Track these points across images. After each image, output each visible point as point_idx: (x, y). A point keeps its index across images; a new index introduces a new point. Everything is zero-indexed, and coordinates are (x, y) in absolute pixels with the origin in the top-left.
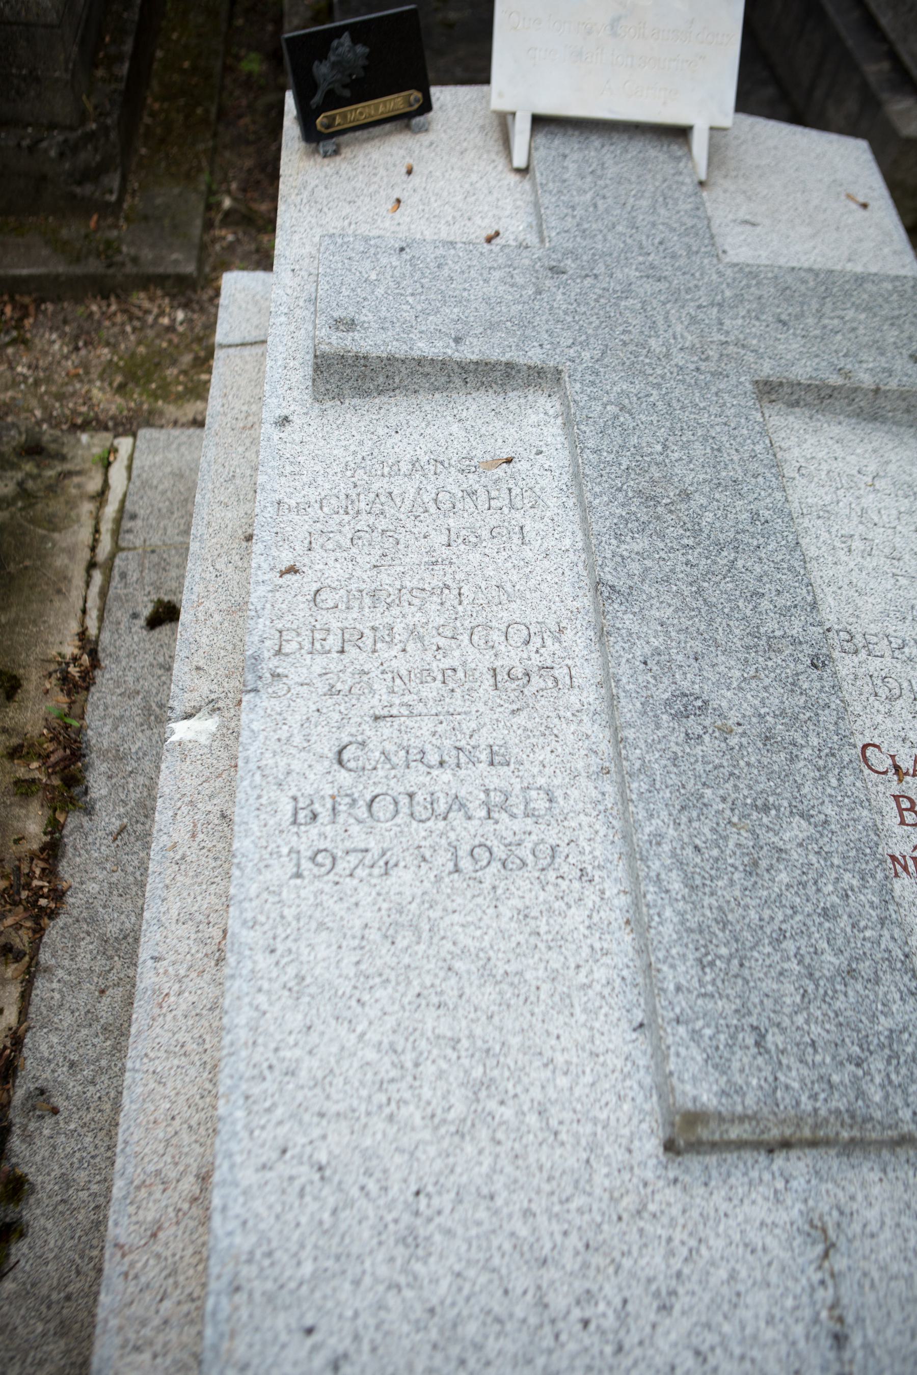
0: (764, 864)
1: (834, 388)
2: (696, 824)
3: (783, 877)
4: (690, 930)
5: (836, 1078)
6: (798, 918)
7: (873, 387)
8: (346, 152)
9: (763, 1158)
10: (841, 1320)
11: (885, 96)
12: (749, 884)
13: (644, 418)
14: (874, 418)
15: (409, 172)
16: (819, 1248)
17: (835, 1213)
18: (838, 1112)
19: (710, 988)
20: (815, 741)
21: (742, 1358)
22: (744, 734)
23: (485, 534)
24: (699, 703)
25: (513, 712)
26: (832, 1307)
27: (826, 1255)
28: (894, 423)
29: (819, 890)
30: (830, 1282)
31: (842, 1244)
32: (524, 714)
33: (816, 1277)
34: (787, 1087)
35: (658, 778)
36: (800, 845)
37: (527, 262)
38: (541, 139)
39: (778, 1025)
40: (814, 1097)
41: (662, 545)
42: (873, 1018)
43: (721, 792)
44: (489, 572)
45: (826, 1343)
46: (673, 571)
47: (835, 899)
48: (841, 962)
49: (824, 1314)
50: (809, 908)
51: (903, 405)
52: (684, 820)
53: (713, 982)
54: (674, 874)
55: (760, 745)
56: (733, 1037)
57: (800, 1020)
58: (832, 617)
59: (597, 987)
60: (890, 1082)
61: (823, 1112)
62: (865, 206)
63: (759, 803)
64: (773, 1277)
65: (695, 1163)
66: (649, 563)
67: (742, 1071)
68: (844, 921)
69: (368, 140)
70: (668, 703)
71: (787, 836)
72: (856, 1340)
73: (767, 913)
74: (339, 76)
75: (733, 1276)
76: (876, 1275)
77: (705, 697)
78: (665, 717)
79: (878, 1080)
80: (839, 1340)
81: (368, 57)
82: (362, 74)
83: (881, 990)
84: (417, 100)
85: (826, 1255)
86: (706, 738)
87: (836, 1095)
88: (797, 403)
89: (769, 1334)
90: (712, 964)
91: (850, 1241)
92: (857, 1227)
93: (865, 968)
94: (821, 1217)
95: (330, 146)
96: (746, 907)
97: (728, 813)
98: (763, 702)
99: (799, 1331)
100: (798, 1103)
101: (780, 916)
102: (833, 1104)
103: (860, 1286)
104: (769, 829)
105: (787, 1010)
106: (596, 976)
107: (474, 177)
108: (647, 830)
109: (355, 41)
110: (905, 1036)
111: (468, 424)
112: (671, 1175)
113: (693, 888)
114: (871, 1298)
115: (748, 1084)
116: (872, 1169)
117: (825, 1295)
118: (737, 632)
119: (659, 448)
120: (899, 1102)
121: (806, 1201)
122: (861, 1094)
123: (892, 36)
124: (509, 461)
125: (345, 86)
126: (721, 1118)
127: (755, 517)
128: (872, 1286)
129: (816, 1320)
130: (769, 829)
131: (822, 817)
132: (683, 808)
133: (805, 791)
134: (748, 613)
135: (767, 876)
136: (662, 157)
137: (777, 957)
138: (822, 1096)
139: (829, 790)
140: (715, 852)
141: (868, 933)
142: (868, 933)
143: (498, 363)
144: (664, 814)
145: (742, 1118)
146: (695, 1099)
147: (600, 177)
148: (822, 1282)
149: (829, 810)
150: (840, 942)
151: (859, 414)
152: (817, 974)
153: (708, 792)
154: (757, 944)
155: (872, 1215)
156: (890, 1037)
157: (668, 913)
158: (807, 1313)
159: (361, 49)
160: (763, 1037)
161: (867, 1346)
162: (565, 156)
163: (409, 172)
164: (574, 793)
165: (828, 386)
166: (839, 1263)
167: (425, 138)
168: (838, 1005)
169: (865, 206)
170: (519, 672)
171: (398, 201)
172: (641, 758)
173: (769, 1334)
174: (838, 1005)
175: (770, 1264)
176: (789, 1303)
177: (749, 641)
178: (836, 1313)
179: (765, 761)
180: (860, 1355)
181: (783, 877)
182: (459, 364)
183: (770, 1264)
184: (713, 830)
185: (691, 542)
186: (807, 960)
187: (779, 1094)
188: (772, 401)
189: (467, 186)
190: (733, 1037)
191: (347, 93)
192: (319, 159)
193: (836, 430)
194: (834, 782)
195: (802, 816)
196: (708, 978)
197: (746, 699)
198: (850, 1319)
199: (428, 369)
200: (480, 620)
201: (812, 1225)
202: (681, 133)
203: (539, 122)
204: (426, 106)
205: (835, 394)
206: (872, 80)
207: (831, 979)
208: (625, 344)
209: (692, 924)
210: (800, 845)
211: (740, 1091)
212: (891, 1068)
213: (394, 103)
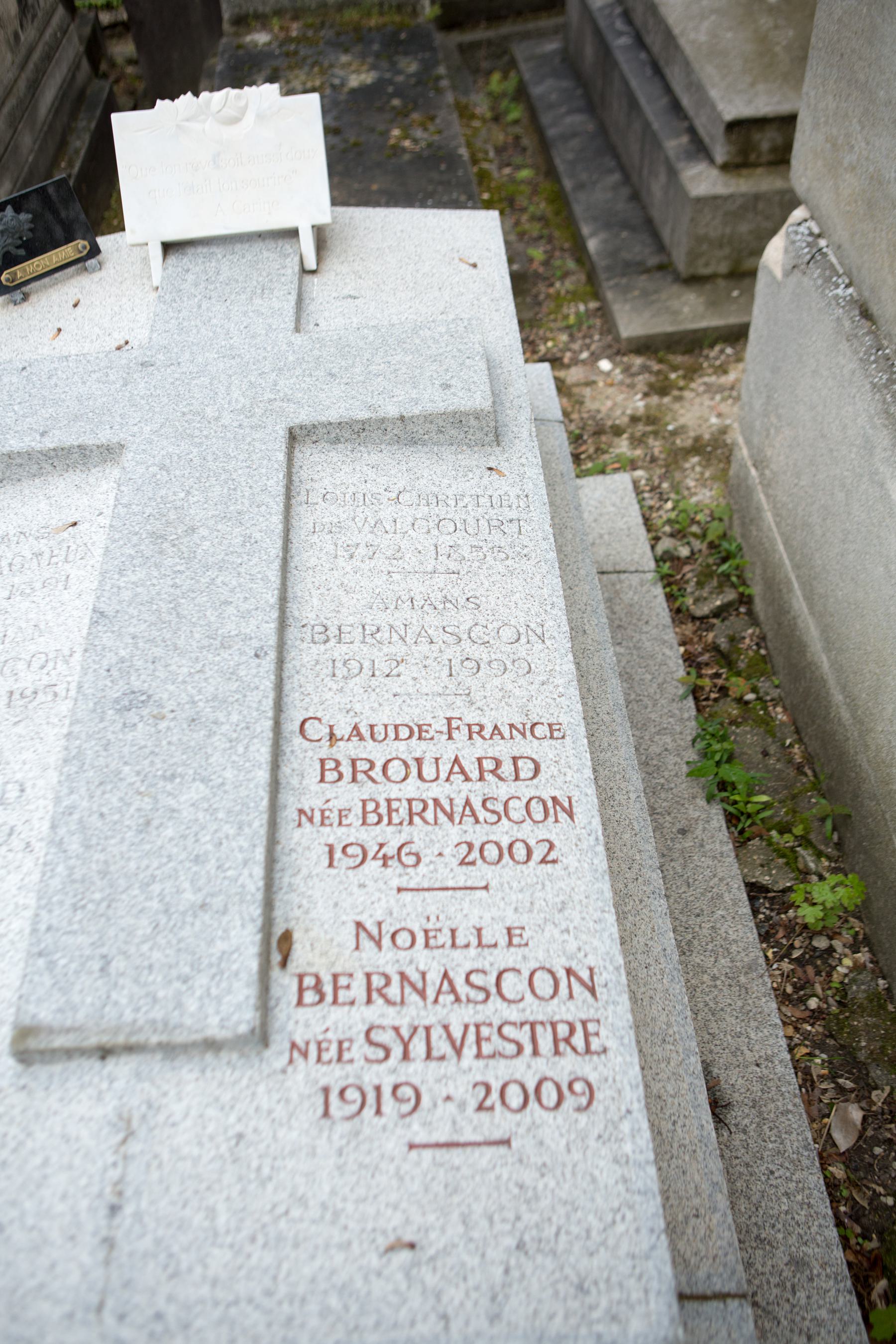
0: (155, 823)
1: (363, 423)
2: (107, 796)
3: (169, 832)
4: (74, 881)
5: (161, 994)
6: (171, 865)
7: (397, 415)
8: (33, 298)
9: (97, 1064)
10: (120, 1194)
11: (680, 165)
12: (137, 840)
13: (178, 473)
14: (413, 442)
15: (75, 305)
16: (121, 1136)
17: (144, 1108)
18: (154, 1022)
19: (76, 927)
20: (235, 718)
21: (33, 1228)
22: (174, 718)
23: (38, 585)
24: (144, 698)
25: (16, 723)
26: (116, 1184)
27: (124, 1141)
28: (434, 444)
29: (197, 841)
30: (120, 1165)
31: (142, 1132)
32: (22, 724)
33: (111, 1159)
34: (116, 1003)
35: (88, 761)
36: (193, 805)
37: (124, 362)
38: (172, 259)
39: (125, 953)
40: (137, 1010)
41: (156, 574)
42: (211, 942)
43: (138, 768)
44: (32, 615)
45: (103, 1212)
46: (158, 594)
47: (209, 847)
48: (199, 898)
49: (108, 1190)
50: (183, 856)
51: (434, 427)
52: (99, 792)
53: (80, 921)
54: (75, 838)
55: (185, 726)
56: (83, 965)
57: (145, 948)
58: (312, 615)
59: (11, 936)
60: (209, 995)
61: (141, 1022)
62: (475, 266)
63: (168, 773)
64: (77, 1161)
65: (42, 1071)
66: (139, 590)
67: (81, 991)
68: (212, 865)
69: (45, 287)
70: (117, 701)
71: (183, 799)
72: (128, 1210)
73: (145, 862)
74: (9, 241)
75: (46, 1162)
76: (165, 1156)
77: (150, 692)
78: (111, 712)
79: (198, 993)
80: (114, 1209)
81: (32, 222)
82: (30, 235)
83: (225, 919)
84: (84, 247)
85: (124, 1141)
86: (140, 725)
87: (157, 1007)
88: (337, 440)
89: (60, 1207)
90: (84, 907)
91: (151, 1130)
92: (161, 1118)
93: (217, 902)
94: (130, 1111)
95: (18, 295)
96: (129, 859)
97: (138, 784)
98: (200, 692)
99: (84, 1204)
100: (121, 1016)
101: (155, 864)
102: (153, 1015)
103: (148, 1165)
104: (170, 794)
105: (136, 940)
106: (12, 927)
107: (124, 300)
108: (65, 804)
109: (18, 210)
110: (236, 956)
111: (53, 501)
112: (22, 1082)
113: (88, 847)
114: (155, 1175)
115: (83, 1002)
116: (191, 1070)
117: (114, 1174)
118: (197, 636)
119: (182, 495)
120: (211, 1011)
121: (121, 1098)
122: (179, 1005)
123: (691, 112)
124: (75, 524)
125: (18, 247)
126: (51, 1031)
127: (247, 538)
128: (160, 1166)
129: (100, 1195)
130: (170, 794)
131: (220, 780)
132: (101, 784)
133: (212, 760)
134: (213, 619)
135: (155, 833)
136: (272, 256)
137: (142, 898)
138: (144, 1009)
139: (234, 758)
140: (116, 817)
141: (229, 873)
142: (229, 873)
143: (71, 447)
144: (83, 791)
145: (68, 1031)
146: (34, 1016)
147: (213, 283)
148: (115, 1164)
149: (229, 774)
150: (201, 883)
151: (398, 440)
152: (173, 910)
153: (127, 769)
154: (128, 888)
155: (178, 1109)
156: (221, 959)
157: (60, 869)
158: (95, 1189)
159: (23, 216)
160: (108, 963)
161: (138, 1216)
162: (188, 271)
163: (75, 305)
164: (41, 783)
165: (357, 422)
166: (134, 1147)
167: (96, 276)
168: (183, 934)
169: (475, 266)
170: (28, 692)
171: (59, 330)
172: (79, 747)
173: (60, 1207)
174: (183, 934)
175: (77, 1151)
176: (83, 1181)
177: (205, 642)
178: (119, 1188)
179: (185, 739)
180: (128, 1222)
181: (169, 832)
182: (41, 452)
183: (77, 1151)
184: (121, 799)
185: (182, 568)
186: (167, 899)
187: (107, 1009)
188: (315, 442)
189: (116, 309)
190: (83, 965)
191: (22, 252)
192: (11, 306)
193: (375, 458)
194: (241, 750)
195: (202, 781)
196: (77, 918)
197: (185, 690)
198: (129, 1192)
199: (19, 461)
200: (13, 654)
201: (120, 1117)
202: (293, 234)
203: (168, 248)
204: (95, 251)
205: (367, 427)
206: (671, 154)
207: (184, 914)
208: (184, 414)
209: (78, 875)
210: (193, 805)
211: (75, 1009)
212: (213, 983)
213: (67, 252)
